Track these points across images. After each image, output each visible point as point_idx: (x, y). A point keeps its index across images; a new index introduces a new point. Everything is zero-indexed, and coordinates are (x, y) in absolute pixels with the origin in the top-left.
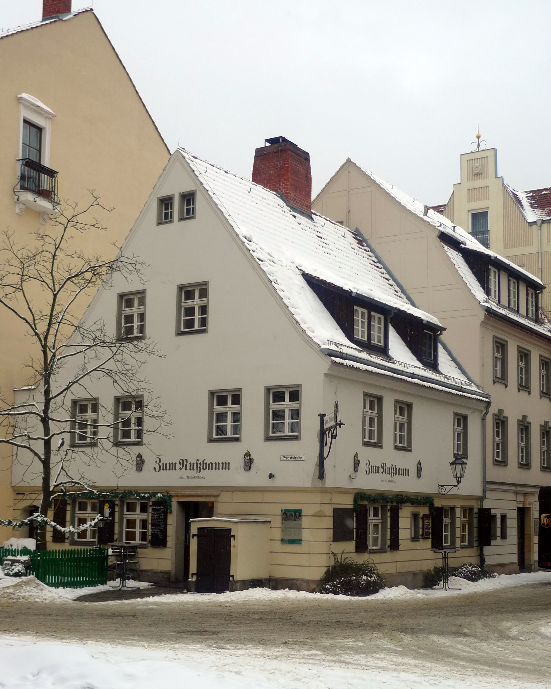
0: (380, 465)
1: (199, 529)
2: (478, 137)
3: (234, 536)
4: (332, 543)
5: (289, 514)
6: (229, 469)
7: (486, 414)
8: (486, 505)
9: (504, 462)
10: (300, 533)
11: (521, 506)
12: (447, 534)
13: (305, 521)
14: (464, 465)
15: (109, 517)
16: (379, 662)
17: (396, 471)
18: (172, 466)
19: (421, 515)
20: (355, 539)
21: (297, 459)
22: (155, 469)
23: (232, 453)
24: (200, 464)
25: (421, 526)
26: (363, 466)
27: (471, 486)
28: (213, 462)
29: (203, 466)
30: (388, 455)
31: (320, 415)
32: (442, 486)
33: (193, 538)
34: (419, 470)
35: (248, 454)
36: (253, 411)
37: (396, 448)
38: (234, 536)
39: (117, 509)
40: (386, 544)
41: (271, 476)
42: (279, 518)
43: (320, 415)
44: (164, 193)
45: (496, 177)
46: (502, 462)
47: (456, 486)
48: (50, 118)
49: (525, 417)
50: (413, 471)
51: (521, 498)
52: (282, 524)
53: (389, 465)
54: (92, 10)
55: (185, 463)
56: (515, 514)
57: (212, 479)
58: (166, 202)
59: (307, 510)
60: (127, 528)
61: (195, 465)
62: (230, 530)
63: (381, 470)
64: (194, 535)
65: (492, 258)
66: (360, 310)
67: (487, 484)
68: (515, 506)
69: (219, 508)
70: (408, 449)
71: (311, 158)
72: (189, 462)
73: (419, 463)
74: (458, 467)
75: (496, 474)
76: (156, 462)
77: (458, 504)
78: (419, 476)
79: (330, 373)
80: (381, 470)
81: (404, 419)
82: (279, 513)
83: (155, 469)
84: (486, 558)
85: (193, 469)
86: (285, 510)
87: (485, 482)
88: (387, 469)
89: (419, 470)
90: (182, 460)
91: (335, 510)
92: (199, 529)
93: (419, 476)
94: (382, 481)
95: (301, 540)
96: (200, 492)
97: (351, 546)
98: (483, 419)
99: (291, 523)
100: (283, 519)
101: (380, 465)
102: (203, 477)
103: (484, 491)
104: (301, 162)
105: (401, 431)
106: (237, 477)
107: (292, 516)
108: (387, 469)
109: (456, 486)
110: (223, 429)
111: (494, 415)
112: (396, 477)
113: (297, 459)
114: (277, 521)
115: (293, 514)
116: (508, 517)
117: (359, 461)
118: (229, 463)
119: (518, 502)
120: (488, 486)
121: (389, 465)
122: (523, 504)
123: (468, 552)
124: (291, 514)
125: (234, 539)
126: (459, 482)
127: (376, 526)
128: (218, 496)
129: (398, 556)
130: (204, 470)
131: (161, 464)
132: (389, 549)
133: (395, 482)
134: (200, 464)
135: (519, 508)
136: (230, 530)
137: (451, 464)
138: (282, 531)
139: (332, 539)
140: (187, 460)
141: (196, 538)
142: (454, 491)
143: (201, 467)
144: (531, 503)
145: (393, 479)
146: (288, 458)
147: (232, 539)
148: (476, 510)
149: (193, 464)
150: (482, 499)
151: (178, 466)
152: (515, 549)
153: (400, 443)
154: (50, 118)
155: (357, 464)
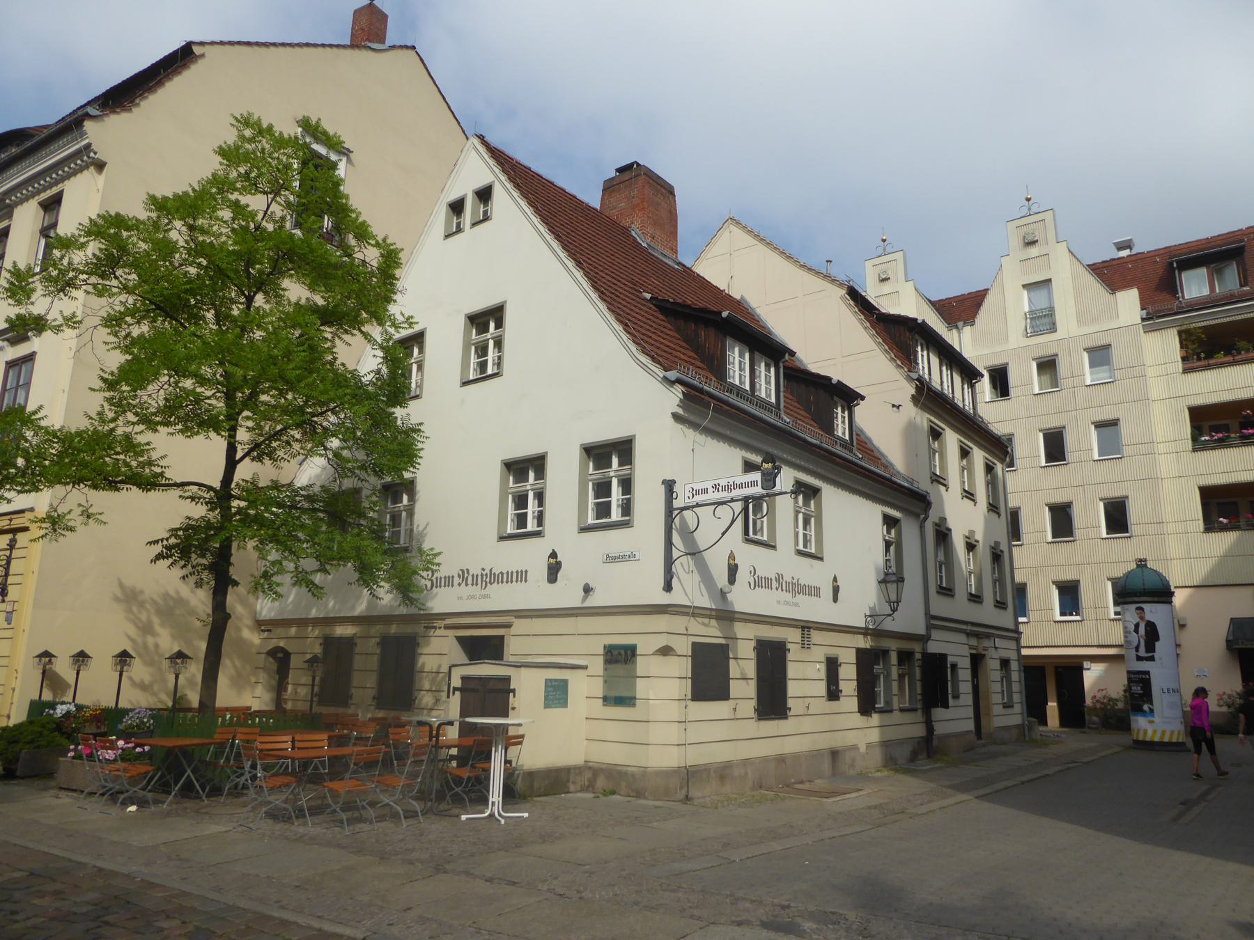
1: (464, 679)
3: (513, 691)
4: (690, 703)
5: (615, 653)
7: (926, 519)
9: (950, 590)
10: (633, 687)
11: (974, 652)
12: (880, 689)
13: (642, 665)
16: (838, 447)
17: (799, 589)
21: (628, 558)
23: (531, 555)
26: (743, 576)
29: (491, 578)
31: (664, 482)
34: (836, 590)
35: (554, 555)
36: (565, 481)
37: (800, 553)
38: (513, 691)
41: (587, 590)
42: (601, 660)
43: (664, 482)
44: (454, 196)
50: (827, 592)
51: (974, 642)
52: (605, 669)
53: (787, 578)
54: (414, 48)
56: (965, 663)
57: (501, 598)
58: (457, 207)
59: (645, 646)
62: (507, 680)
63: (775, 584)
64: (455, 689)
67: (933, 621)
68: (966, 651)
69: (513, 647)
73: (835, 579)
74: (892, 587)
75: (941, 606)
78: (835, 600)
79: (680, 411)
80: (775, 584)
82: (601, 651)
84: (936, 726)
86: (610, 646)
87: (930, 617)
89: (836, 590)
91: (694, 644)
93: (835, 600)
94: (778, 602)
96: (485, 620)
98: (922, 527)
99: (619, 669)
100: (607, 662)
102: (486, 596)
103: (929, 627)
105: (805, 529)
106: (537, 594)
107: (620, 657)
110: (523, 520)
112: (800, 597)
113: (628, 558)
115: (623, 652)
119: (971, 647)
121: (787, 578)
123: (908, 717)
126: (894, 610)
128: (509, 626)
133: (796, 605)
135: (972, 655)
136: (507, 680)
138: (605, 682)
139: (689, 696)
141: (458, 693)
144: (986, 649)
145: (795, 600)
148: (918, 656)
151: (456, 580)
152: (970, 712)
153: (805, 546)
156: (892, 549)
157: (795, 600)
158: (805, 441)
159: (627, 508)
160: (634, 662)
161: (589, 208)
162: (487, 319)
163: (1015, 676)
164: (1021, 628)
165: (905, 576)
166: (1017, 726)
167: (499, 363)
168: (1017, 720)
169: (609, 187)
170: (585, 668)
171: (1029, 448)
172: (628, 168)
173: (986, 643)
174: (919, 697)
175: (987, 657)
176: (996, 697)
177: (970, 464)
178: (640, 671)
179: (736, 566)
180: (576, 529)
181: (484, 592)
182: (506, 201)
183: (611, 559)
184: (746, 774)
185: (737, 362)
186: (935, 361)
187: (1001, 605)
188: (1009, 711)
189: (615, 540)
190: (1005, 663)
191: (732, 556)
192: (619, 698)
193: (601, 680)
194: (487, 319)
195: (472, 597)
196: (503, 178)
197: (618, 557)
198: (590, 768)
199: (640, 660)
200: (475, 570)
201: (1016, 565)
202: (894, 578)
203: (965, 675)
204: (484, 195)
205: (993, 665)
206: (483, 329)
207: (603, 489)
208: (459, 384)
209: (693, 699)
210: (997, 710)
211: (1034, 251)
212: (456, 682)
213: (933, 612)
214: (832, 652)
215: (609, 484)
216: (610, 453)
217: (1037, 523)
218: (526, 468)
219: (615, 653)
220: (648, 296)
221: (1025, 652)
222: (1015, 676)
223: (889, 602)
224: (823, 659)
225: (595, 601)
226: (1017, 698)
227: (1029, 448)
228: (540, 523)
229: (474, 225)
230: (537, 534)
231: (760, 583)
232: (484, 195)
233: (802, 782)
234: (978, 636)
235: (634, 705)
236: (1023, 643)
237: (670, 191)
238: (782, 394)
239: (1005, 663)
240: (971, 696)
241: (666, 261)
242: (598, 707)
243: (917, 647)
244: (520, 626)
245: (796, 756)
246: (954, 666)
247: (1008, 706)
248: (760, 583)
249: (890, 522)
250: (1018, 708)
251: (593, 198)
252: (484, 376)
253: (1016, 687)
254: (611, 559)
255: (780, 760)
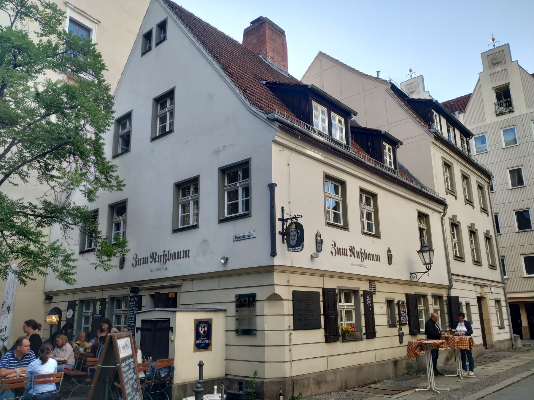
0: (347, 247)
1: (143, 322)
2: (411, 71)
4: (292, 332)
6: (189, 257)
7: (444, 215)
8: (454, 293)
11: (479, 295)
14: (431, 253)
15: (100, 314)
18: (145, 261)
19: (396, 301)
20: (323, 325)
21: (249, 237)
22: (133, 264)
24: (166, 255)
25: (397, 312)
26: (327, 247)
27: (438, 275)
28: (176, 252)
29: (169, 256)
30: (354, 237)
32: (413, 273)
33: (137, 332)
39: (107, 307)
40: (79, 308)
41: (226, 260)
42: (234, 305)
45: (425, 92)
46: (460, 258)
47: (426, 272)
48: (96, 23)
49: (473, 224)
50: (384, 258)
51: (478, 289)
52: (237, 311)
53: (357, 249)
55: (155, 256)
56: (474, 302)
57: (175, 269)
59: (261, 294)
60: (84, 325)
61: (162, 257)
63: (349, 253)
64: (138, 329)
65: (434, 101)
66: (320, 108)
68: (475, 295)
69: (182, 299)
70: (377, 236)
71: (286, 34)
72: (157, 255)
73: (389, 251)
74: (426, 255)
76: (332, 245)
77: (429, 292)
78: (390, 263)
80: (349, 253)
81: (371, 209)
82: (234, 299)
83: (133, 264)
85: (161, 261)
86: (239, 295)
87: (450, 274)
88: (355, 253)
90: (153, 253)
91: (294, 293)
92: (143, 322)
93: (390, 263)
94: (352, 264)
95: (256, 330)
96: (166, 284)
97: (319, 334)
99: (245, 311)
101: (347, 247)
103: (450, 281)
104: (277, 34)
108: (355, 253)
109: (426, 272)
111: (450, 219)
112: (366, 262)
113: (249, 237)
114: (232, 309)
115: (247, 299)
116: (471, 304)
117: (322, 241)
118: (189, 251)
120: (453, 277)
121: (357, 249)
122: (481, 294)
124: (245, 300)
125: (172, 331)
127: (349, 313)
128: (179, 286)
129: (375, 343)
130: (169, 260)
131: (137, 260)
132: (365, 337)
133: (364, 266)
134: (166, 255)
137: (418, 252)
138: (237, 319)
139: (292, 328)
140: (156, 253)
141: (139, 332)
142: (425, 279)
143: (167, 258)
144: (486, 294)
145: (363, 263)
146: (240, 237)
147: (170, 331)
148: (445, 298)
149: (161, 256)
150: (450, 287)
151: (150, 260)
154: (96, 23)
155: (320, 243)
156: (425, 233)
157: (363, 263)
158: (364, 163)
159: (247, 205)
160: (254, 306)
161: (236, 42)
162: (165, 100)
163: (504, 310)
164: (505, 282)
165: (434, 247)
166: (507, 340)
167: (171, 125)
168: (507, 336)
169: (247, 33)
170: (225, 311)
171: (502, 179)
172: (258, 20)
173: (486, 290)
174: (447, 324)
175: (487, 299)
176: (494, 323)
177: (469, 185)
178: (258, 311)
179: (322, 241)
180: (217, 221)
181: (164, 266)
182: (176, 30)
183: (238, 239)
184: (336, 379)
185: (319, 113)
186: (444, 122)
187: (492, 267)
188: (502, 331)
189: (240, 227)
190: (498, 301)
191: (318, 235)
192: (246, 330)
193: (234, 318)
194: (165, 100)
195: (158, 269)
196: (172, 14)
197: (242, 237)
198: (228, 379)
199: (258, 304)
200: (160, 253)
201: (500, 246)
202: (427, 249)
203: (475, 310)
204: (162, 26)
205: (491, 303)
206: (163, 106)
207: (233, 195)
208: (149, 139)
209: (295, 329)
210: (495, 330)
211: (498, 68)
212: (138, 324)
213: (453, 271)
214: (390, 296)
215: (237, 191)
216: (236, 173)
217: (509, 222)
218: (187, 187)
219: (243, 300)
220: (264, 82)
221: (509, 296)
222: (504, 310)
223: (425, 264)
224: (384, 301)
225: (232, 265)
226: (506, 323)
227: (502, 179)
228: (197, 220)
229: (157, 44)
230: (195, 227)
231: (339, 252)
232: (162, 26)
233: (375, 382)
234: (481, 286)
235: (255, 334)
236: (508, 290)
237: (282, 33)
238: (350, 138)
239: (498, 301)
240: (478, 315)
241: (282, 73)
242: (234, 338)
243: (444, 292)
244: (187, 286)
245: (370, 365)
246: (467, 304)
247: (501, 327)
248: (339, 252)
249: (422, 216)
250: (507, 329)
251: (239, 38)
252: (164, 133)
253: (505, 316)
254: (238, 239)
255: (359, 368)
